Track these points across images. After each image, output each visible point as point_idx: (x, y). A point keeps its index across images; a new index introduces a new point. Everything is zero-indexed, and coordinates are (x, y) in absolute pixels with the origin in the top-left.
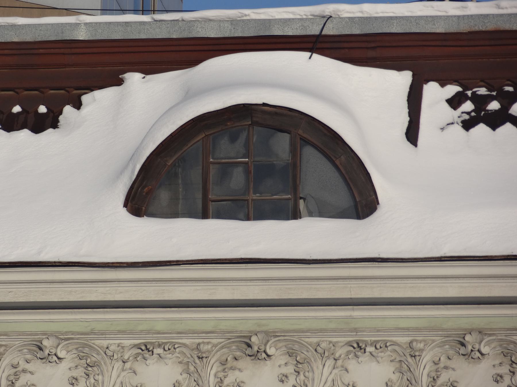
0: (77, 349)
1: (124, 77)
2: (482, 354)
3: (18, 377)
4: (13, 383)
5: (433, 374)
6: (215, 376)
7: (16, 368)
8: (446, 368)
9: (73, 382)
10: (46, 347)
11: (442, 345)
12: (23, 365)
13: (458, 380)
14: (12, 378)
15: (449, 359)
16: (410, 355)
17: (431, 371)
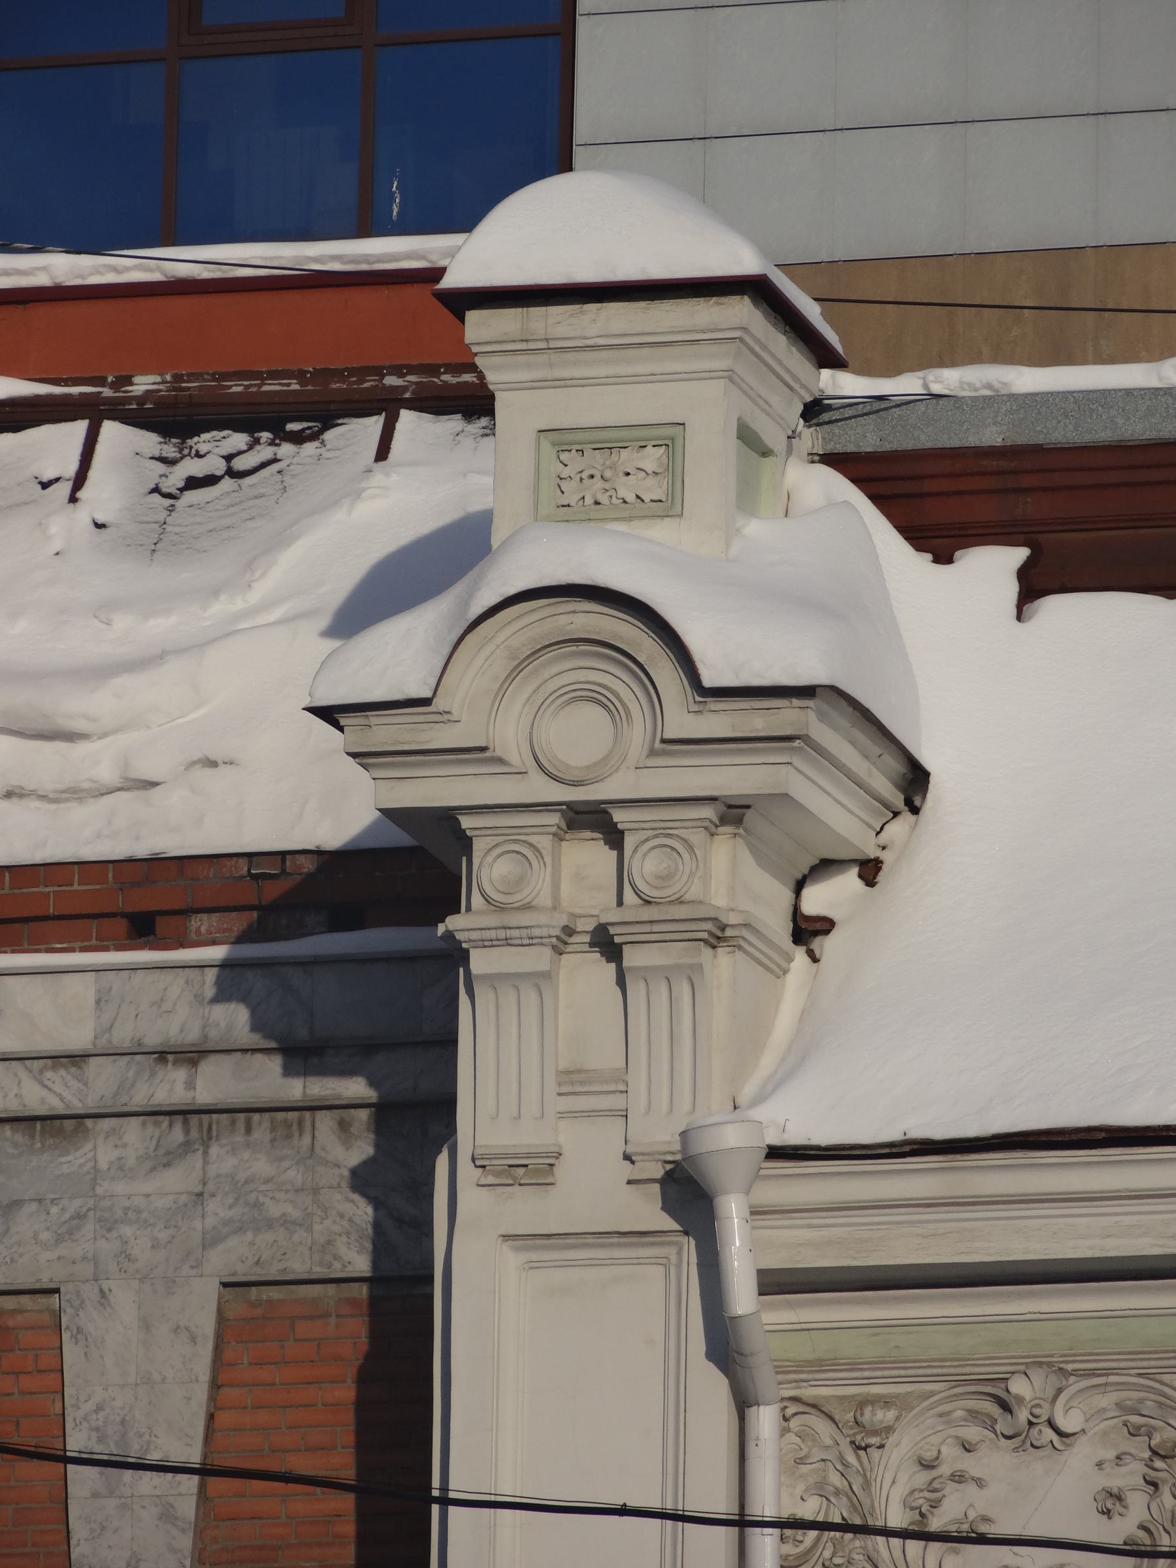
1: (449, 935)
3: (939, 1495)
4: (922, 1515)
7: (933, 1467)
8: (958, 1478)
9: (1109, 1506)
10: (1020, 1400)
12: (952, 1459)
13: (991, 1515)
14: (921, 1501)
15: (968, 1451)
16: (853, 1442)
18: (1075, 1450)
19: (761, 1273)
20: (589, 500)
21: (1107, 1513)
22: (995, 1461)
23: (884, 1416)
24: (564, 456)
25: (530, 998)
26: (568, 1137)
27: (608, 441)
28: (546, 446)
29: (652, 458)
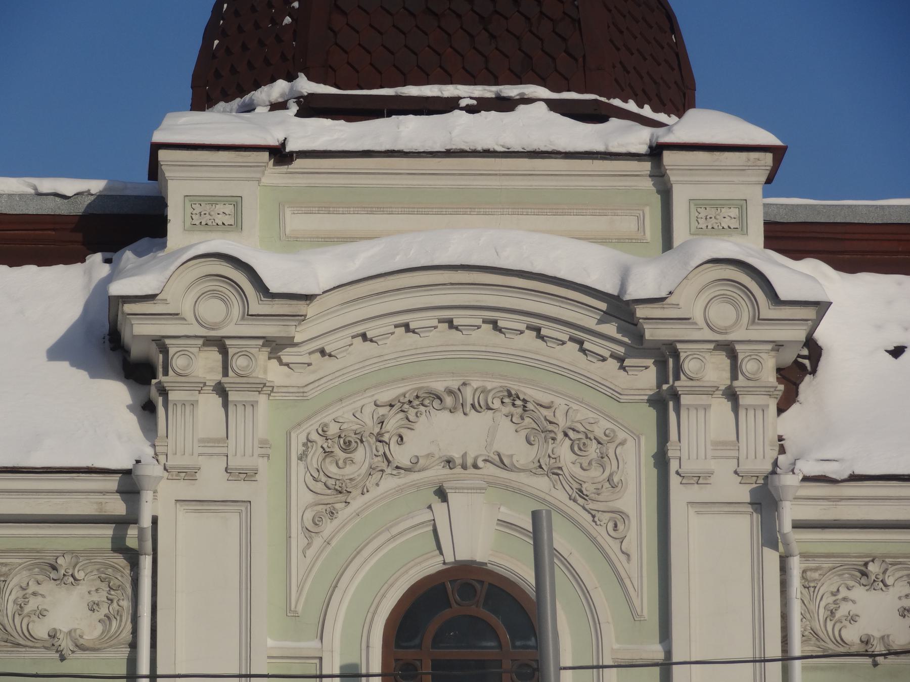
0: (98, 570)
2: (75, 579)
4: (21, 607)
5: (832, 606)
6: (15, 602)
8: (35, 594)
11: (29, 568)
17: (17, 598)
18: (79, 587)
19: (793, 521)
20: (710, 227)
21: (93, 611)
22: (859, 593)
23: (816, 575)
24: (699, 210)
25: (701, 413)
26: (202, 461)
27: (718, 204)
28: (692, 206)
29: (734, 212)
